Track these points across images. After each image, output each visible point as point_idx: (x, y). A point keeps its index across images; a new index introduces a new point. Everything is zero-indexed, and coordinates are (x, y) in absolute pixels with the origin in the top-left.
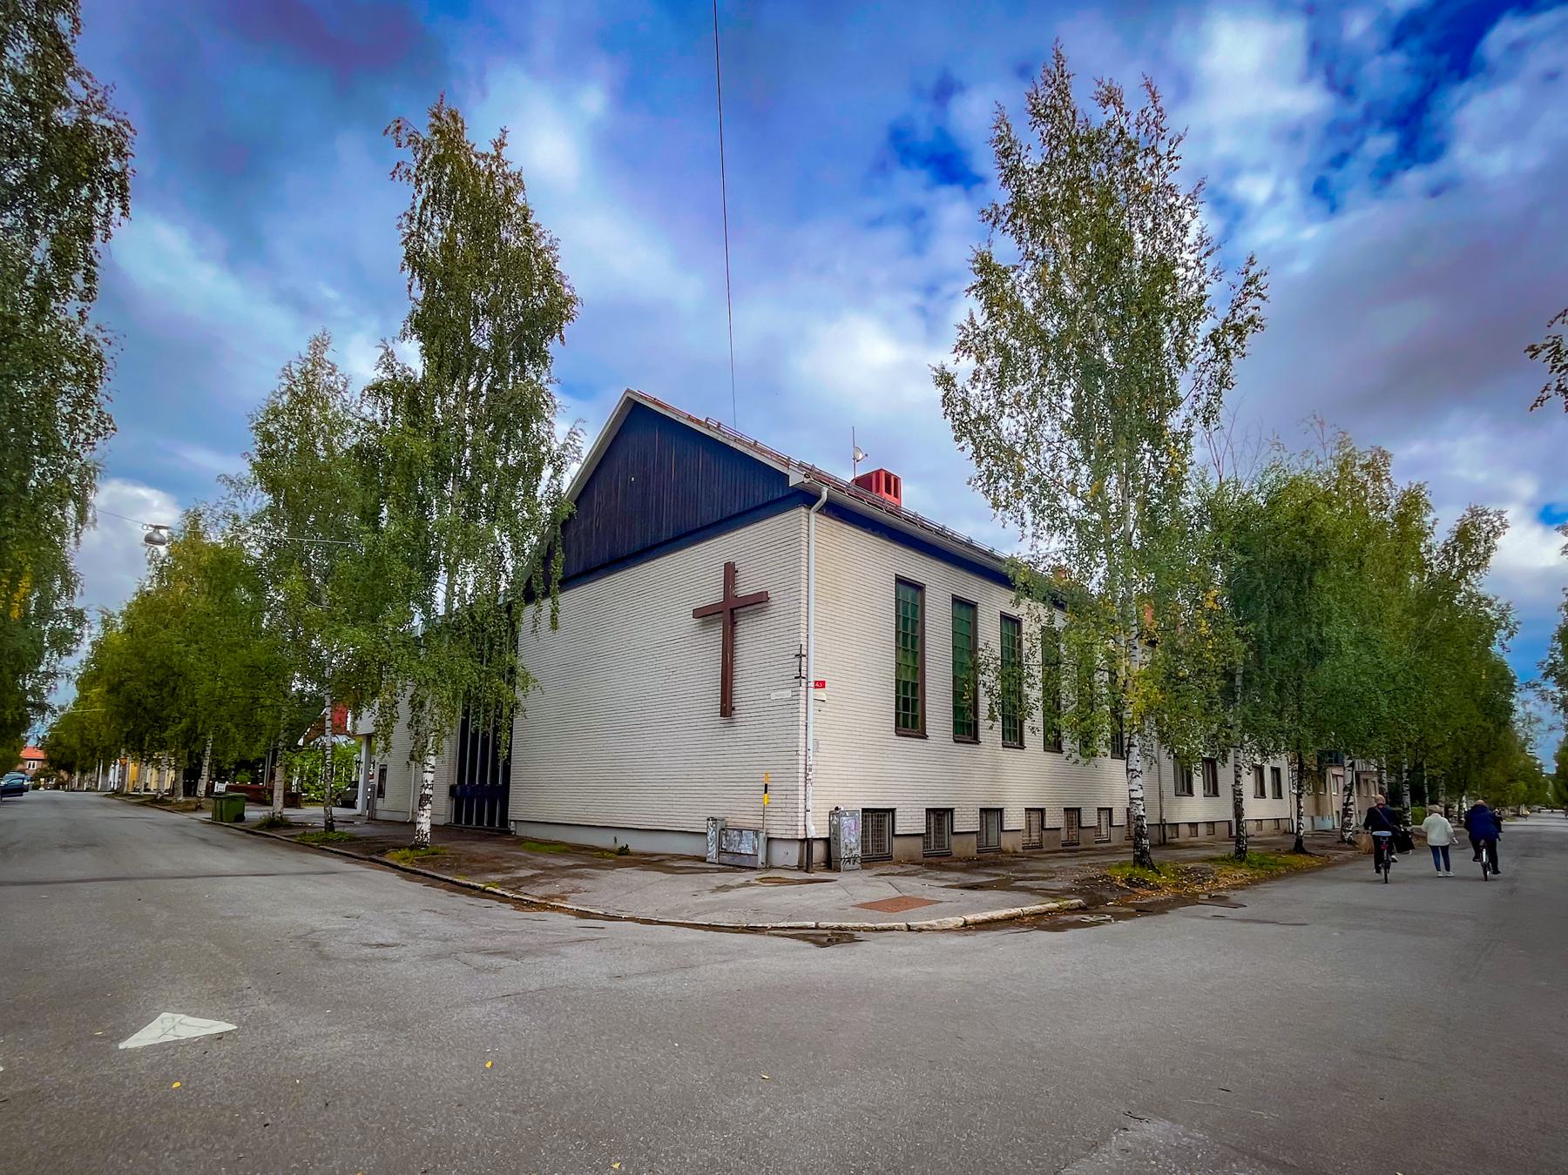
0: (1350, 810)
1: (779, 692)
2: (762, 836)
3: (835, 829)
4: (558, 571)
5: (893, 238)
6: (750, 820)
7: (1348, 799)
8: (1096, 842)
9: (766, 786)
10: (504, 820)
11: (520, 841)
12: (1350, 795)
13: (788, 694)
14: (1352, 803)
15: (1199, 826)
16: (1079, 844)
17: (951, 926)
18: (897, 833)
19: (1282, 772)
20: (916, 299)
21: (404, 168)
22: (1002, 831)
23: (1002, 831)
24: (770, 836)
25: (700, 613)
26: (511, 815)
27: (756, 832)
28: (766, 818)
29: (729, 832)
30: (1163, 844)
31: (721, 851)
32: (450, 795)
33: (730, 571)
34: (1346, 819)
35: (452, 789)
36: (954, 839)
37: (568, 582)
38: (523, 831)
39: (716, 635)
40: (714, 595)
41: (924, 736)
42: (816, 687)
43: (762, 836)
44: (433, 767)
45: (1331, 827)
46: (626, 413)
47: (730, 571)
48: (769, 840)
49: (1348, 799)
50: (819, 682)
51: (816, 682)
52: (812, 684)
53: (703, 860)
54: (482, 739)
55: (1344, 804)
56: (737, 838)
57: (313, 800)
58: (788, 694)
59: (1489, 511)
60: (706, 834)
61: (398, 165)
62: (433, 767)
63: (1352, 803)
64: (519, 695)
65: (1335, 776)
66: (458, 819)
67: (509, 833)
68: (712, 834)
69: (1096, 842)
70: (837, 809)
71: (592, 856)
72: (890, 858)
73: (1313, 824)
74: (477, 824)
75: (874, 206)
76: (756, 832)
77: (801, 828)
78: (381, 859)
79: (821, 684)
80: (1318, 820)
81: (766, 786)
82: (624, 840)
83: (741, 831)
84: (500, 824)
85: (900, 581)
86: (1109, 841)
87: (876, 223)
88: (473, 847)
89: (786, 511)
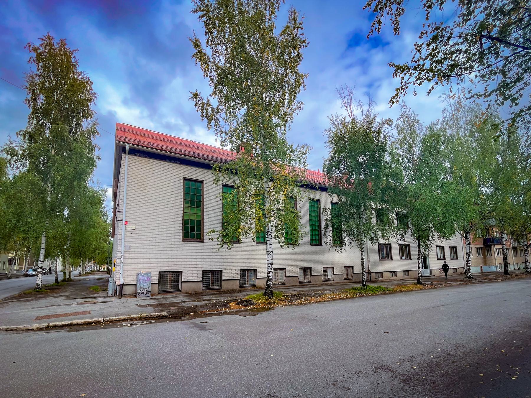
0: (469, 263)
5: (355, 71)
7: (468, 259)
8: (323, 281)
12: (469, 257)
14: (470, 261)
15: (409, 271)
16: (310, 282)
17: (34, 328)
19: (458, 249)
20: (365, 90)
21: (32, 59)
22: (256, 278)
23: (256, 278)
30: (370, 280)
36: (223, 283)
45: (495, 270)
49: (468, 259)
55: (467, 261)
59: (78, 64)
61: (31, 58)
63: (470, 261)
65: (498, 249)
69: (323, 281)
72: (180, 291)
73: (482, 270)
75: (348, 61)
80: (484, 268)
85: (185, 179)
86: (333, 281)
87: (349, 66)
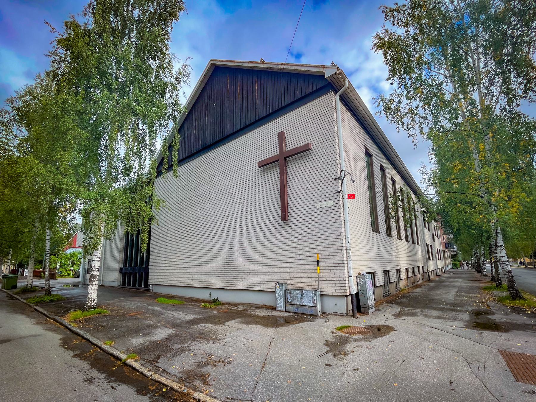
1: (323, 203)
2: (318, 294)
3: (362, 289)
4: (176, 158)
6: (304, 283)
9: (318, 261)
10: (147, 285)
11: (156, 296)
13: (331, 203)
18: (377, 285)
24: (323, 294)
25: (264, 165)
26: (150, 281)
27: (315, 292)
28: (320, 282)
29: (293, 291)
31: (286, 303)
32: (120, 272)
33: (282, 136)
34: (484, 267)
35: (121, 269)
37: (181, 162)
38: (156, 290)
39: (274, 175)
40: (272, 151)
41: (379, 233)
42: (349, 198)
43: (318, 294)
44: (99, 258)
46: (212, 71)
47: (282, 136)
48: (321, 295)
50: (351, 195)
51: (348, 195)
52: (346, 196)
53: (274, 309)
54: (131, 238)
56: (299, 296)
57: (64, 275)
58: (331, 203)
60: (275, 292)
62: (99, 258)
64: (154, 212)
66: (124, 284)
67: (149, 291)
68: (279, 293)
70: (359, 274)
71: (199, 306)
74: (133, 286)
76: (315, 292)
77: (348, 291)
78: (56, 318)
79: (352, 196)
81: (318, 261)
82: (215, 295)
83: (302, 291)
84: (144, 285)
88: (128, 303)
89: (319, 97)
